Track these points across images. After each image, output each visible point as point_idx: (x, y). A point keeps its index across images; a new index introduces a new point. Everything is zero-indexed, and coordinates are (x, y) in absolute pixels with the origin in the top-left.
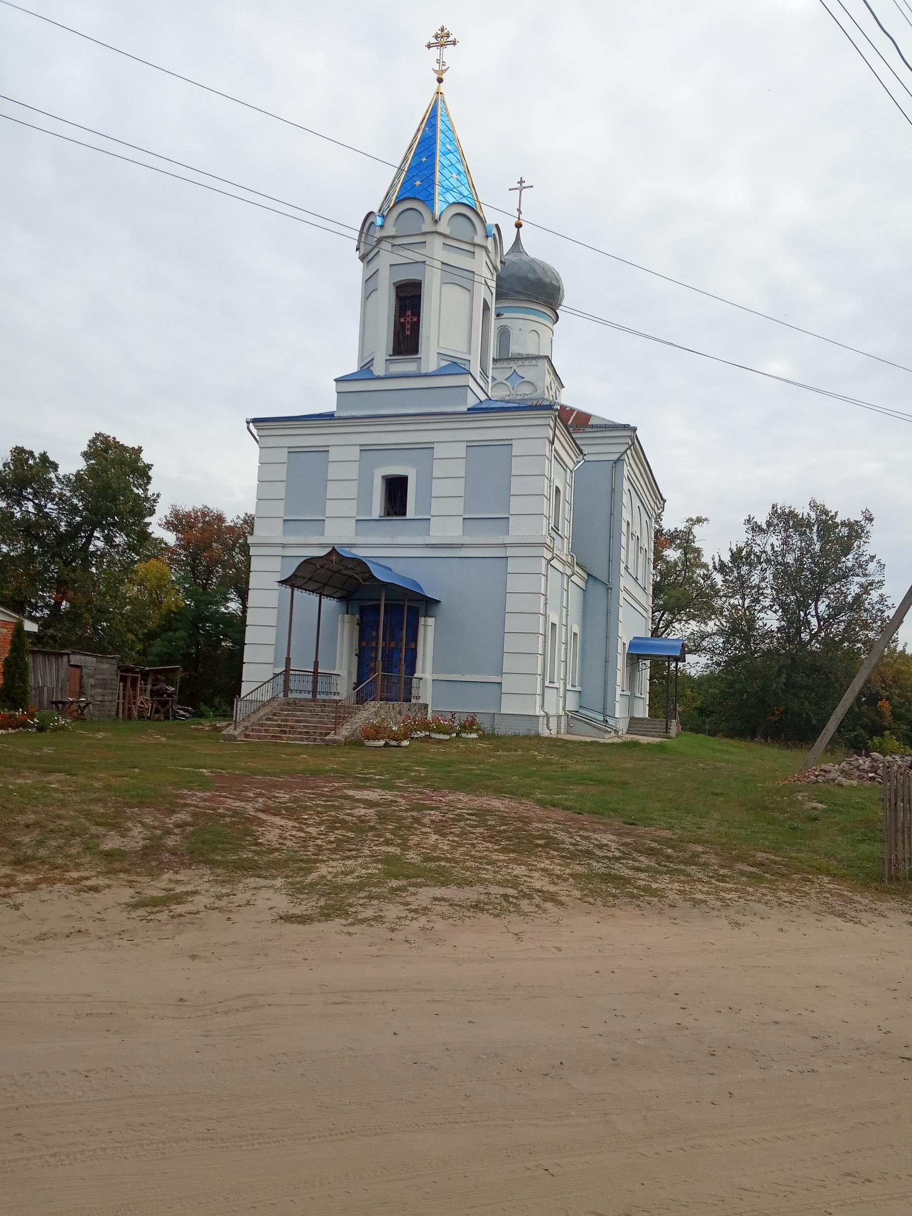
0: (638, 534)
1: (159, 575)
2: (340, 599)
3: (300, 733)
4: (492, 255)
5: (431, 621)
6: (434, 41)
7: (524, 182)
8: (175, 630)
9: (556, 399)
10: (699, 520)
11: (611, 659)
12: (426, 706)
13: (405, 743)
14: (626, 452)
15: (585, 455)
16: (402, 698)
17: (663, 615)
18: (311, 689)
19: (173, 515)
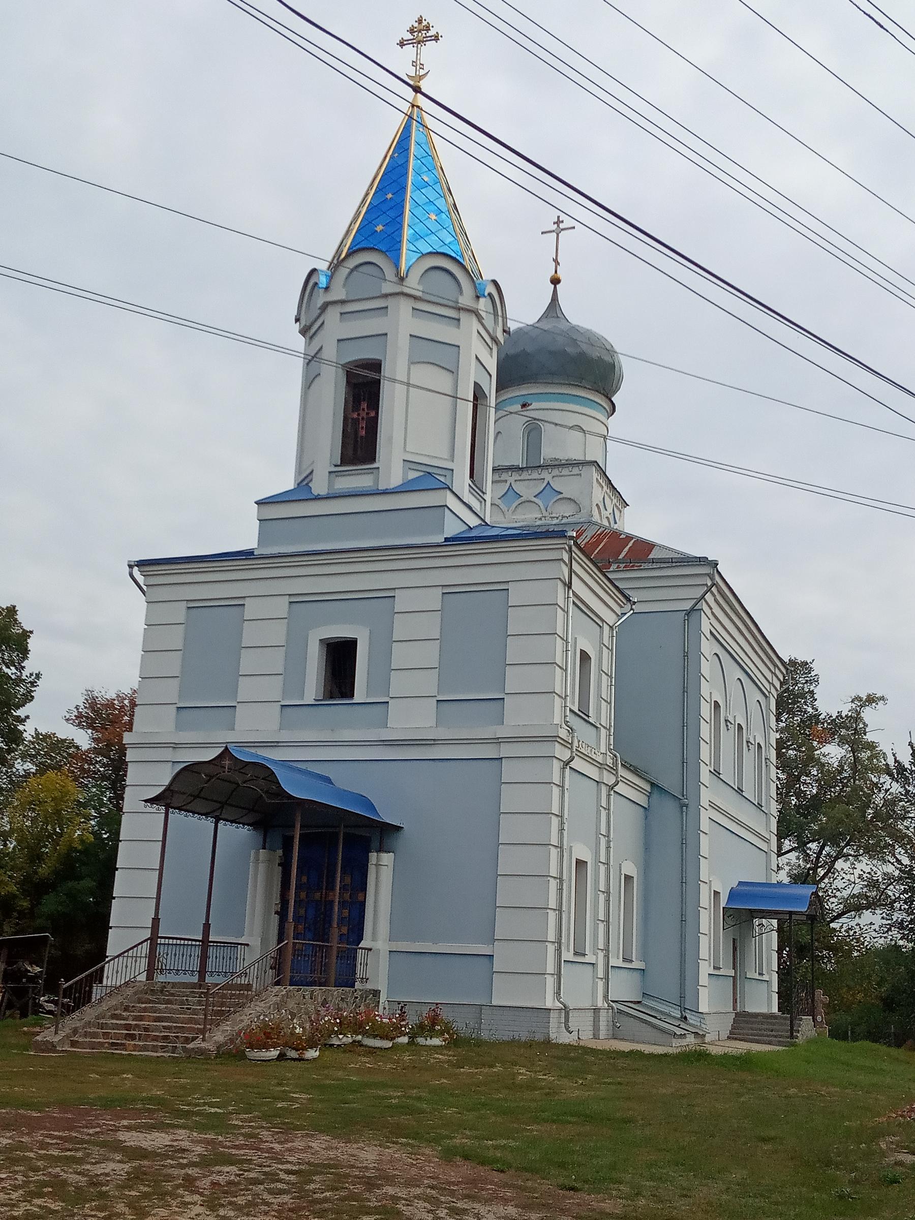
0: (741, 720)
1: (58, 794)
2: (255, 825)
3: (156, 1039)
4: (488, 320)
5: (387, 858)
6: (409, 36)
7: (562, 222)
8: (79, 878)
9: (616, 523)
10: (871, 700)
11: (690, 918)
12: (376, 993)
13: (312, 1054)
14: (703, 597)
15: (634, 603)
16: (333, 979)
17: (822, 848)
18: (196, 968)
19: (87, 706)
